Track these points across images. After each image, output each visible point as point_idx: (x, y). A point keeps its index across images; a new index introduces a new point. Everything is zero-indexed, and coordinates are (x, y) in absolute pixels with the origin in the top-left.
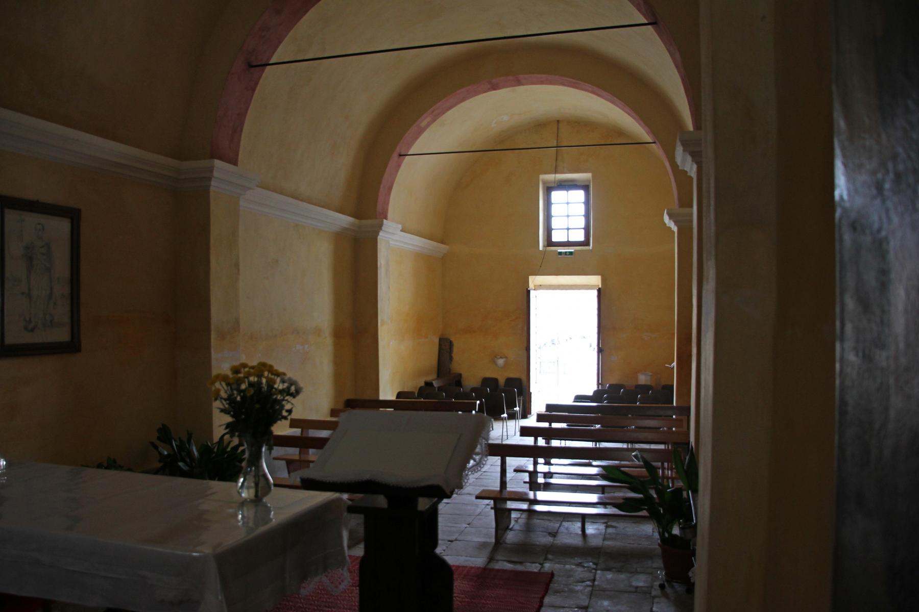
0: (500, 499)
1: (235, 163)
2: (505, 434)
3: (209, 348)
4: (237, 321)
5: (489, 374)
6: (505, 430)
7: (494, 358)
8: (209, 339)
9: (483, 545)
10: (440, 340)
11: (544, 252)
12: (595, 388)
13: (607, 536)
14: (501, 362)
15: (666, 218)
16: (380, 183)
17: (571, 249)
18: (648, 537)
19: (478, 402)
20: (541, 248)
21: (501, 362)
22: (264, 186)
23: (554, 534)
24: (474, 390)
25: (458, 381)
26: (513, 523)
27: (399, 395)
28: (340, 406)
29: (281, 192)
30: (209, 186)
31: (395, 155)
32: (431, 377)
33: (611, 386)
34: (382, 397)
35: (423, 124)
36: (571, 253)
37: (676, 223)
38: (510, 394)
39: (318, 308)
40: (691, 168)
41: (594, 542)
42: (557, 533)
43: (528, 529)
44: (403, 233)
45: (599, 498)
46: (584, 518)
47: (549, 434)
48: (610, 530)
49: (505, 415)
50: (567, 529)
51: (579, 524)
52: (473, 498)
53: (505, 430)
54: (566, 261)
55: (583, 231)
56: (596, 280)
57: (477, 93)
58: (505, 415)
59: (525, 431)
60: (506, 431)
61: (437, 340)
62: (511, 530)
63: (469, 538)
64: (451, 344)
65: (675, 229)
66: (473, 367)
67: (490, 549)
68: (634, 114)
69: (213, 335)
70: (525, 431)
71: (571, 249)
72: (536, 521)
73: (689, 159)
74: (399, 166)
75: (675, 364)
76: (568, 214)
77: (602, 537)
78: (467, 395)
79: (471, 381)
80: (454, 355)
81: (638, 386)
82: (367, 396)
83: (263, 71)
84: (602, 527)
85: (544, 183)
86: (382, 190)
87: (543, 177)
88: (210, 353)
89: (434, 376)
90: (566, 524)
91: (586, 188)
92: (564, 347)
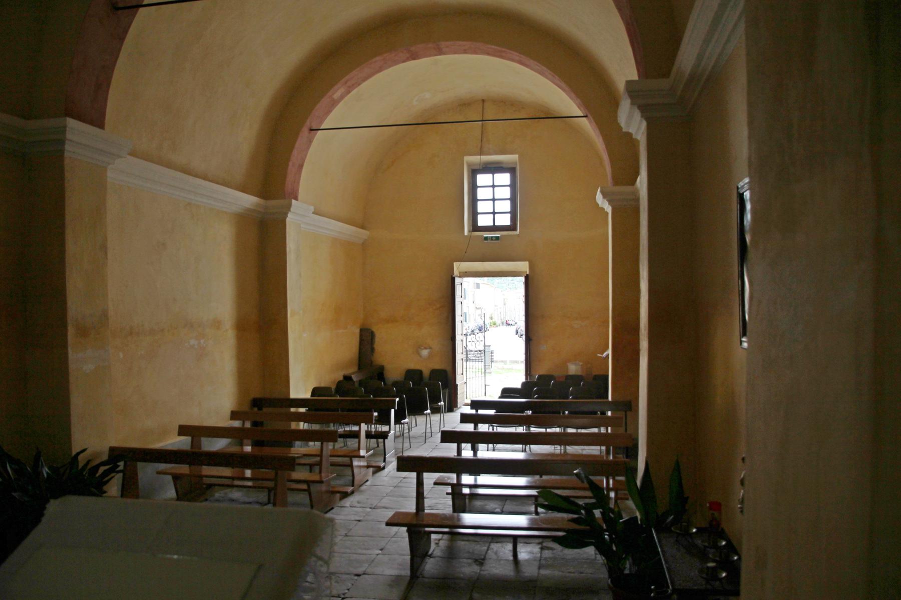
0: (417, 527)
1: (101, 126)
2: (429, 430)
3: (64, 346)
4: (105, 314)
5: (413, 366)
6: (428, 426)
7: (418, 348)
8: (65, 335)
9: (397, 579)
10: (361, 330)
11: (470, 237)
12: (524, 380)
13: (543, 562)
14: (425, 353)
15: (599, 197)
16: (288, 160)
17: (498, 234)
18: (591, 562)
19: (397, 399)
20: (466, 233)
21: (425, 353)
22: (133, 154)
23: (480, 561)
24: (395, 384)
25: (380, 374)
26: (433, 546)
27: (315, 392)
28: (246, 408)
29: (170, 165)
30: (62, 151)
31: (305, 130)
32: (351, 370)
33: (540, 377)
34: (293, 395)
35: (336, 96)
36: (497, 238)
37: (610, 202)
38: (432, 388)
39: (217, 296)
40: (638, 129)
41: (530, 571)
42: (484, 559)
43: (451, 554)
44: (317, 217)
45: (531, 520)
46: (515, 539)
47: (475, 439)
48: (547, 554)
49: (429, 411)
50: (496, 553)
51: (510, 546)
52: (384, 526)
53: (428, 426)
54: (492, 250)
55: (509, 215)
56: (524, 266)
57: (396, 63)
58: (429, 411)
59: (448, 437)
60: (424, 434)
61: (358, 331)
62: (430, 556)
63: (378, 570)
64: (372, 335)
65: (608, 209)
66: (399, 355)
67: (403, 587)
68: (564, 85)
69: (71, 331)
70: (448, 437)
71: (498, 234)
72: (461, 544)
73: (637, 115)
74: (310, 142)
75: (610, 351)
76: (493, 199)
77: (537, 563)
78: (386, 392)
79: (395, 369)
80: (375, 346)
81: (568, 377)
82: (276, 395)
83: (134, 15)
84: (536, 549)
85: (469, 165)
86: (292, 169)
87: (467, 159)
88: (66, 354)
89: (355, 369)
90: (495, 546)
91: (512, 170)
92: (492, 339)
